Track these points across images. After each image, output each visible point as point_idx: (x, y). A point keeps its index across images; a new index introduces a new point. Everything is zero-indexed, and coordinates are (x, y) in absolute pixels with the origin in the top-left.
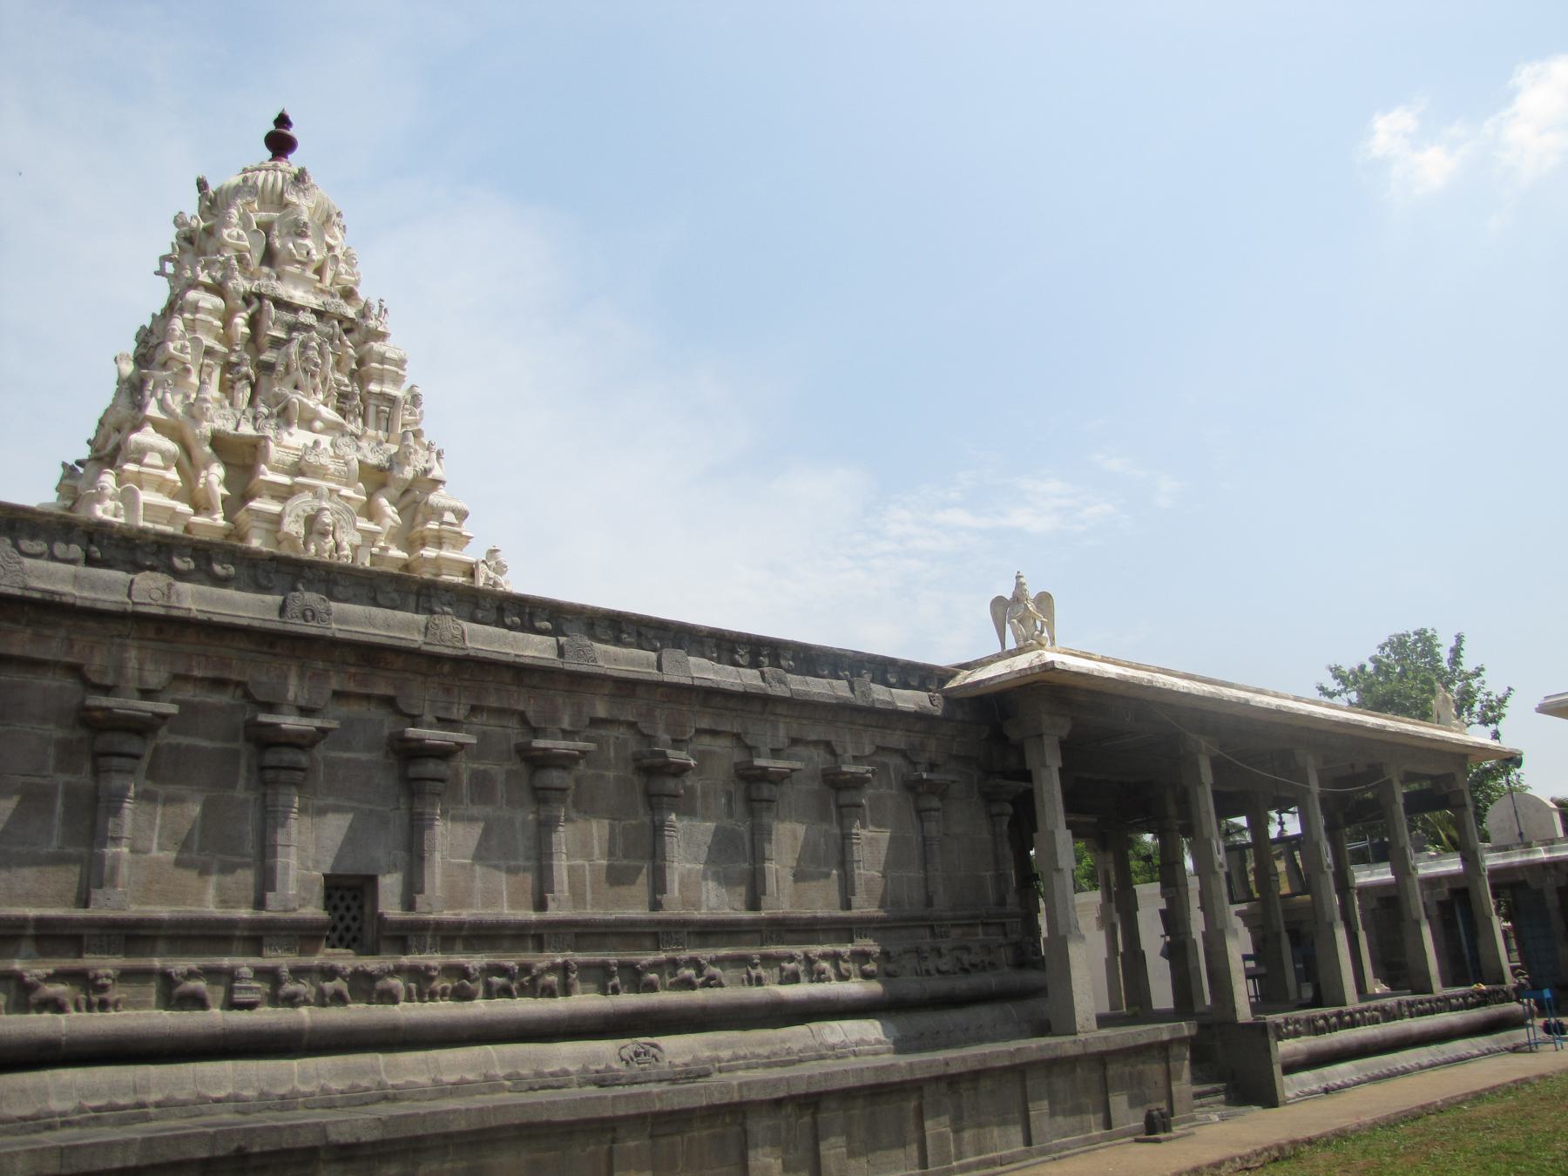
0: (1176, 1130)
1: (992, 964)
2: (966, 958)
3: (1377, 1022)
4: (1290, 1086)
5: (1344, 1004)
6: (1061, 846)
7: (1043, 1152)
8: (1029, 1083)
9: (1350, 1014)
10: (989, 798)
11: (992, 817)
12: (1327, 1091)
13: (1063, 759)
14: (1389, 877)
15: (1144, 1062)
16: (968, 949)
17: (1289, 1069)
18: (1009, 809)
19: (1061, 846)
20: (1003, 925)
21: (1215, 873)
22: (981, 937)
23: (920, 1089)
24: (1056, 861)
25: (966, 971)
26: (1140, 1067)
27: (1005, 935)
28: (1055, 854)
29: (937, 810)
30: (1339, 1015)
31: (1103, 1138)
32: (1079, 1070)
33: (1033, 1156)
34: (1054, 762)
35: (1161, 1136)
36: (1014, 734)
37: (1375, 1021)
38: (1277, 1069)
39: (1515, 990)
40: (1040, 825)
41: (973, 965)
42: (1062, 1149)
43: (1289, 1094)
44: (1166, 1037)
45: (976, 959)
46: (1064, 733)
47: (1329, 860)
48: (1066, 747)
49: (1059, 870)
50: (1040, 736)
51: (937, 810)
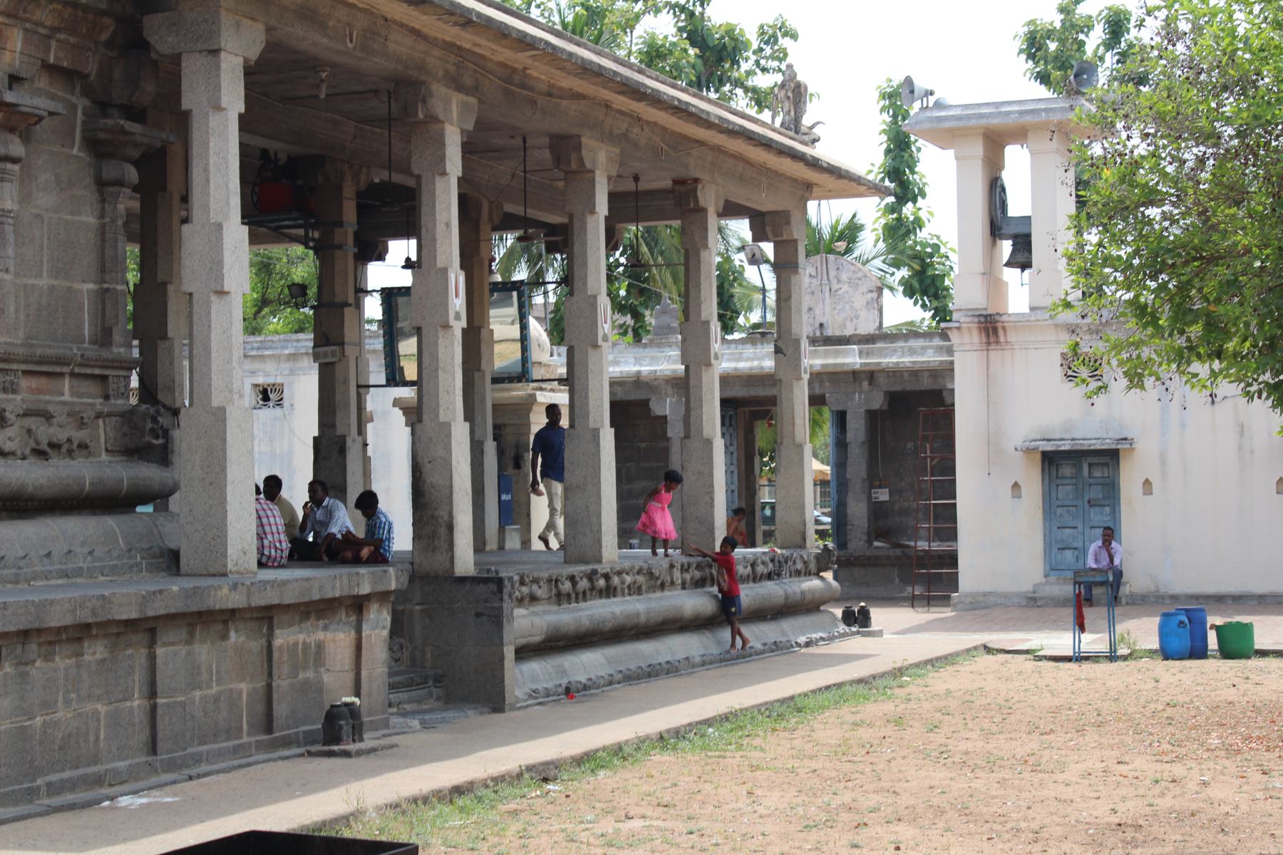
0: (369, 741)
1: (83, 446)
2: (45, 433)
3: (639, 591)
4: (522, 677)
5: (599, 561)
6: (225, 249)
7: (171, 766)
8: (160, 651)
9: (607, 577)
10: (98, 148)
11: (102, 184)
12: (568, 692)
13: (248, 99)
14: (769, 364)
15: (325, 628)
16: (48, 417)
17: (524, 653)
18: (132, 174)
19: (225, 249)
20: (104, 378)
21: (446, 326)
22: (67, 397)
23: (152, 631)
24: (220, 278)
25: (40, 453)
26: (321, 635)
27: (107, 397)
28: (220, 263)
29: (15, 161)
30: (591, 576)
31: (260, 747)
32: (233, 634)
33: (156, 771)
34: (234, 100)
35: (351, 747)
36: (162, 37)
37: (636, 590)
38: (509, 652)
39: (818, 557)
40: (196, 212)
41: (55, 446)
42: (199, 761)
43: (519, 693)
44: (365, 589)
45: (61, 435)
46: (254, 53)
47: (458, 303)
48: (256, 77)
49: (222, 293)
50: (215, 52)
51: (15, 161)
